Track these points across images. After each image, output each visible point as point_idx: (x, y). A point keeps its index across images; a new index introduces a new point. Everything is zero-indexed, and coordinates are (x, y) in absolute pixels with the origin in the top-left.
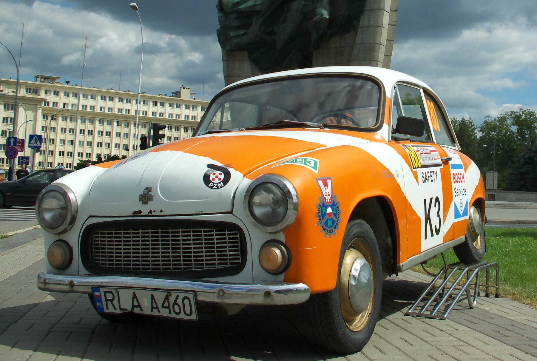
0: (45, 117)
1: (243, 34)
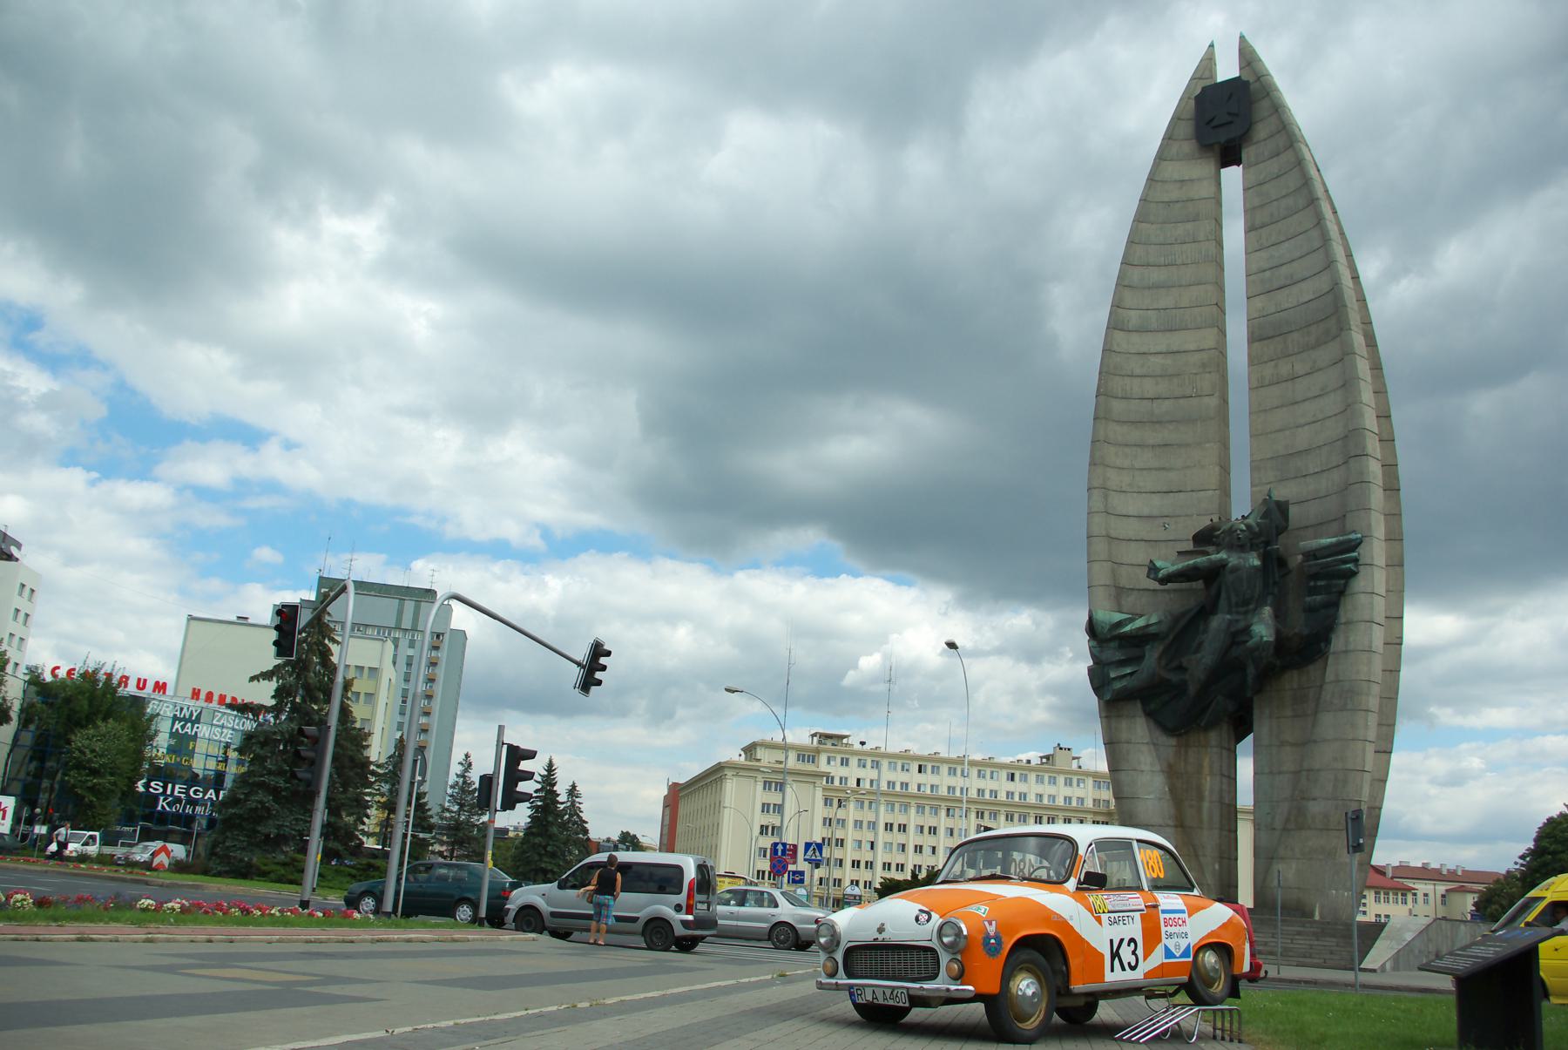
0: (827, 801)
1: (1131, 674)
